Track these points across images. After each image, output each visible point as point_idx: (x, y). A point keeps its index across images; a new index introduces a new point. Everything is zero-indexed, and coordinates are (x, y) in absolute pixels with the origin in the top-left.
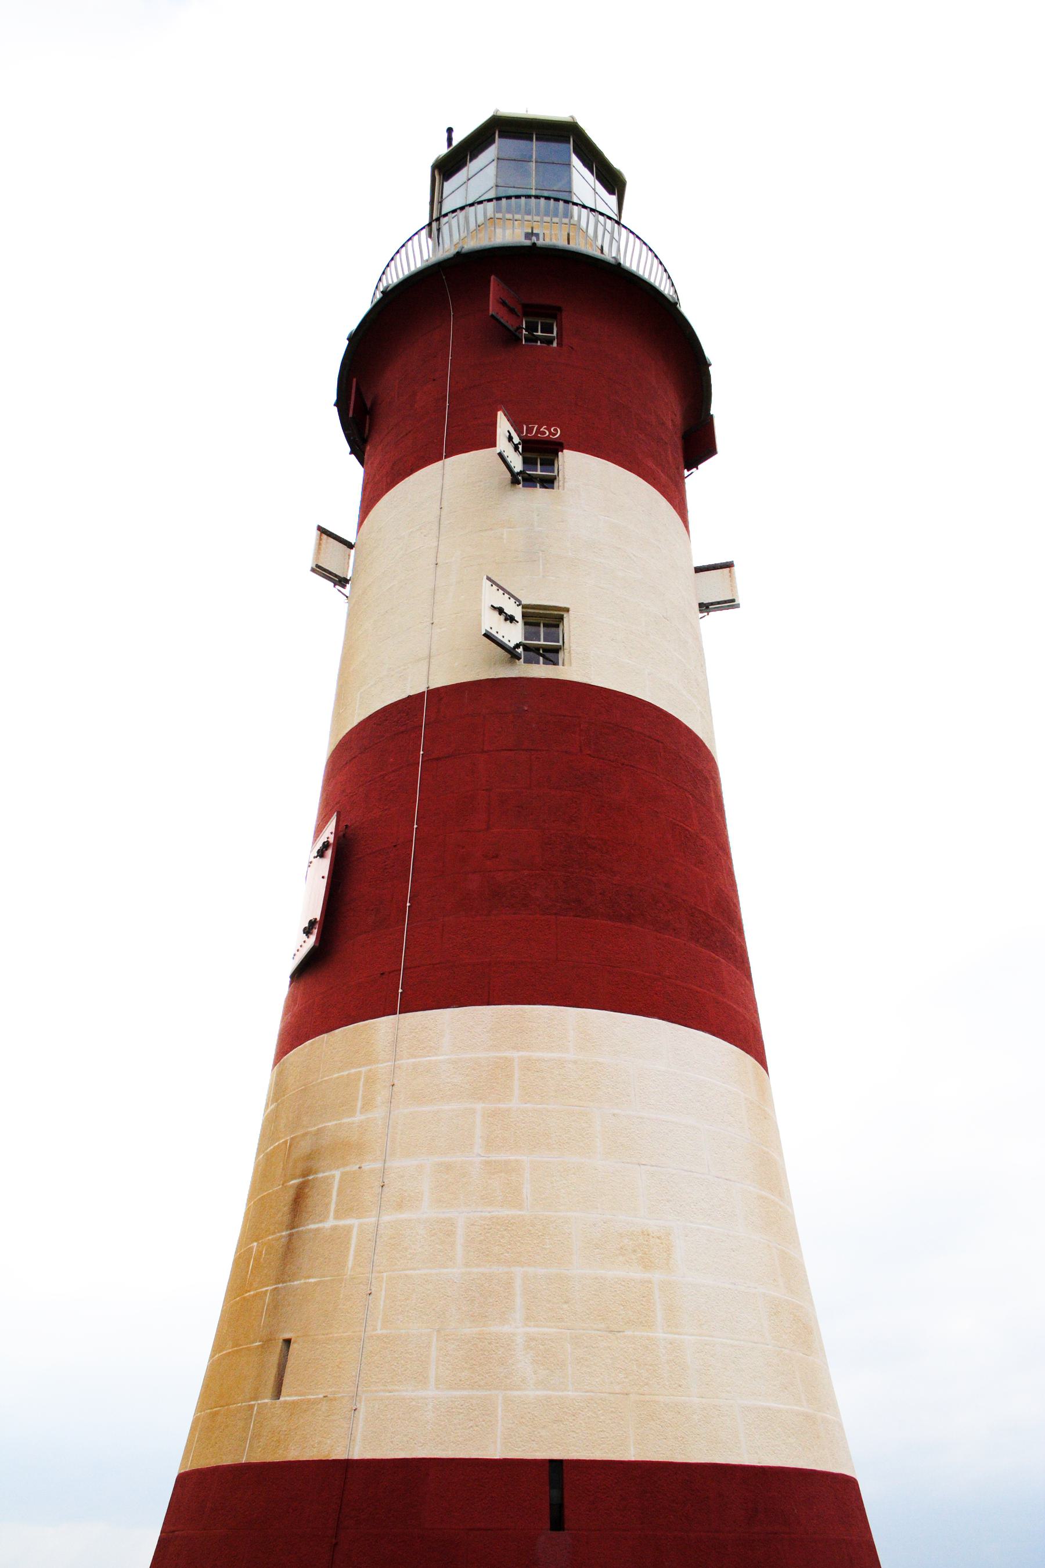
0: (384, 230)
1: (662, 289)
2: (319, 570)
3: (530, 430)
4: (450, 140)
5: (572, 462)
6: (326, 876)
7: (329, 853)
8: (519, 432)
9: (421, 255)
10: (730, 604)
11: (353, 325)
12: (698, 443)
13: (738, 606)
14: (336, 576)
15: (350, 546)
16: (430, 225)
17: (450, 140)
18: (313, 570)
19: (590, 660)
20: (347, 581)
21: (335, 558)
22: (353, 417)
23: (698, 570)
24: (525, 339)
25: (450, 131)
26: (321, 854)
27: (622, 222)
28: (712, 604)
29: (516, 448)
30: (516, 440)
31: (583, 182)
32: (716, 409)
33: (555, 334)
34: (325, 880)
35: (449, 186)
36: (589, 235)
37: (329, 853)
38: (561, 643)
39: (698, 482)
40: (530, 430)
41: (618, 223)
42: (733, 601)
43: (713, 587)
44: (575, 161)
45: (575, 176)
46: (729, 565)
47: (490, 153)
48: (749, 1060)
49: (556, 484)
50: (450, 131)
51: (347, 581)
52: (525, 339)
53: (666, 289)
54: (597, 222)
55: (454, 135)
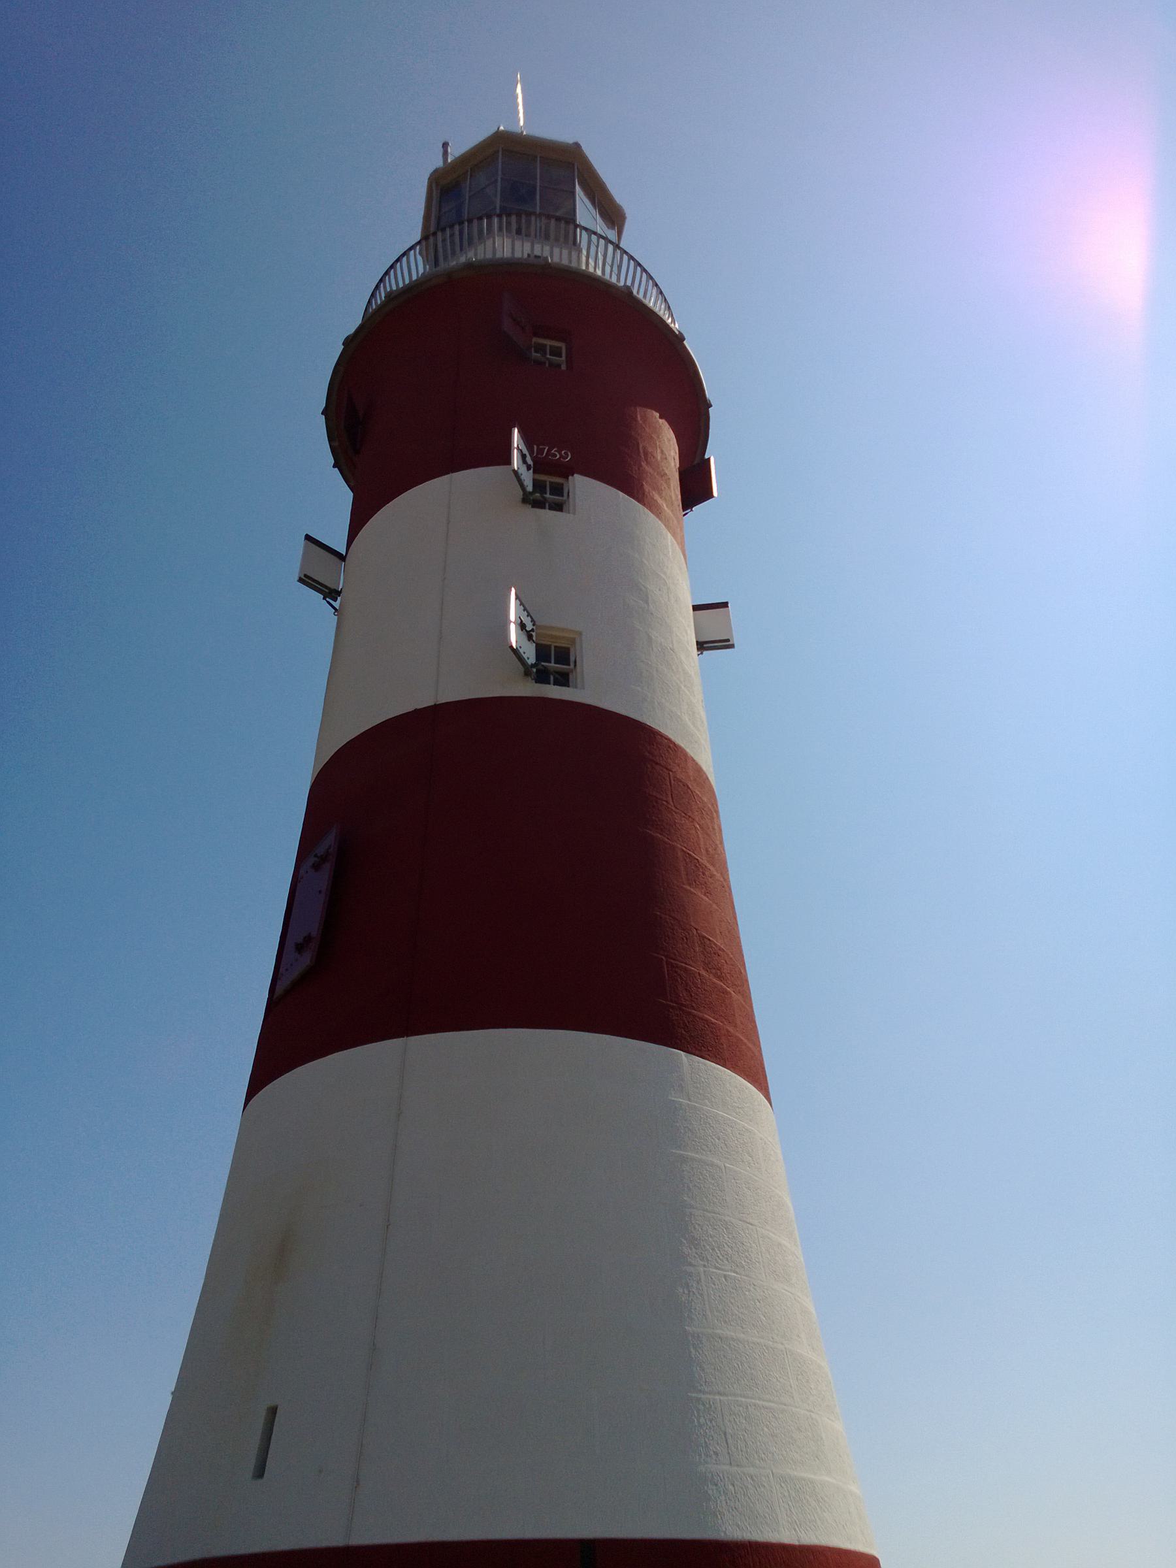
1: (656, 310)
2: (306, 580)
3: (540, 451)
4: (445, 153)
5: (582, 487)
7: (327, 867)
9: (417, 267)
11: (352, 329)
13: (732, 646)
14: (326, 587)
15: (342, 558)
17: (445, 153)
18: (300, 580)
19: (592, 689)
20: (339, 593)
26: (316, 867)
29: (529, 468)
30: (529, 460)
33: (564, 358)
36: (594, 261)
38: (572, 666)
40: (540, 451)
41: (617, 247)
42: (728, 640)
46: (725, 605)
49: (565, 507)
50: (445, 145)
51: (339, 593)
54: (589, 238)
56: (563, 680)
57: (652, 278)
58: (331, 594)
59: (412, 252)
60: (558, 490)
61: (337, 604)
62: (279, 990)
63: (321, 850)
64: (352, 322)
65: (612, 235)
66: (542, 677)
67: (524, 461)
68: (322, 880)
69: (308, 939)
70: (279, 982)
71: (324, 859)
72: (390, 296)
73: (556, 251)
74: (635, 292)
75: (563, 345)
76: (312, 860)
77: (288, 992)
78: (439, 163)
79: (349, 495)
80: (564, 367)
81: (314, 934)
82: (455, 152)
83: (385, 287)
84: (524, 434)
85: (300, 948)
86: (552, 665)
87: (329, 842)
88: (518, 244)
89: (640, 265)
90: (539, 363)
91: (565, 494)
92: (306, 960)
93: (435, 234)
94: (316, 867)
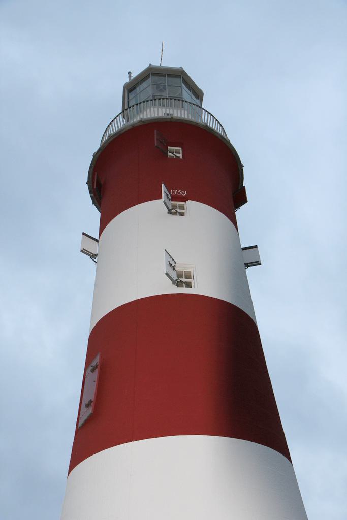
0: (99, 113)
2: (84, 251)
3: (174, 192)
4: (130, 76)
6: (96, 381)
7: (97, 371)
8: (170, 193)
9: (121, 124)
10: (257, 263)
11: (96, 150)
12: (240, 198)
13: (260, 264)
14: (91, 253)
15: (97, 241)
16: (123, 111)
18: (82, 251)
20: (96, 256)
21: (94, 248)
22: (161, 184)
23: (243, 249)
24: (166, 153)
25: (130, 73)
26: (93, 371)
27: (202, 107)
28: (249, 263)
29: (170, 200)
31: (187, 94)
32: (246, 183)
34: (95, 383)
35: (132, 95)
37: (97, 371)
39: (240, 213)
40: (174, 192)
41: (201, 107)
42: (258, 261)
43: (249, 256)
44: (183, 85)
45: (184, 91)
46: (256, 247)
47: (150, 81)
48: (286, 459)
50: (130, 73)
51: (96, 256)
52: (166, 153)
53: (220, 131)
55: (132, 75)
56: (189, 285)
57: (219, 123)
58: (93, 256)
59: (121, 115)
60: (182, 207)
61: (96, 260)
62: (80, 424)
63: (94, 363)
64: (96, 146)
65: (198, 101)
66: (179, 284)
67: (168, 197)
68: (95, 376)
69: (91, 401)
70: (80, 421)
71: (96, 367)
72: (110, 136)
73: (175, 111)
74: (209, 125)
75: (180, 149)
76: (90, 368)
77: (84, 425)
78: (127, 80)
79: (99, 214)
80: (181, 158)
81: (93, 400)
82: (134, 75)
83: (108, 133)
84: (166, 186)
85: (88, 406)
86: (184, 280)
87: (96, 361)
88: (160, 109)
89: (210, 113)
90: (172, 158)
91: (192, 278)
92: (90, 411)
93: (126, 109)
94: (93, 371)
